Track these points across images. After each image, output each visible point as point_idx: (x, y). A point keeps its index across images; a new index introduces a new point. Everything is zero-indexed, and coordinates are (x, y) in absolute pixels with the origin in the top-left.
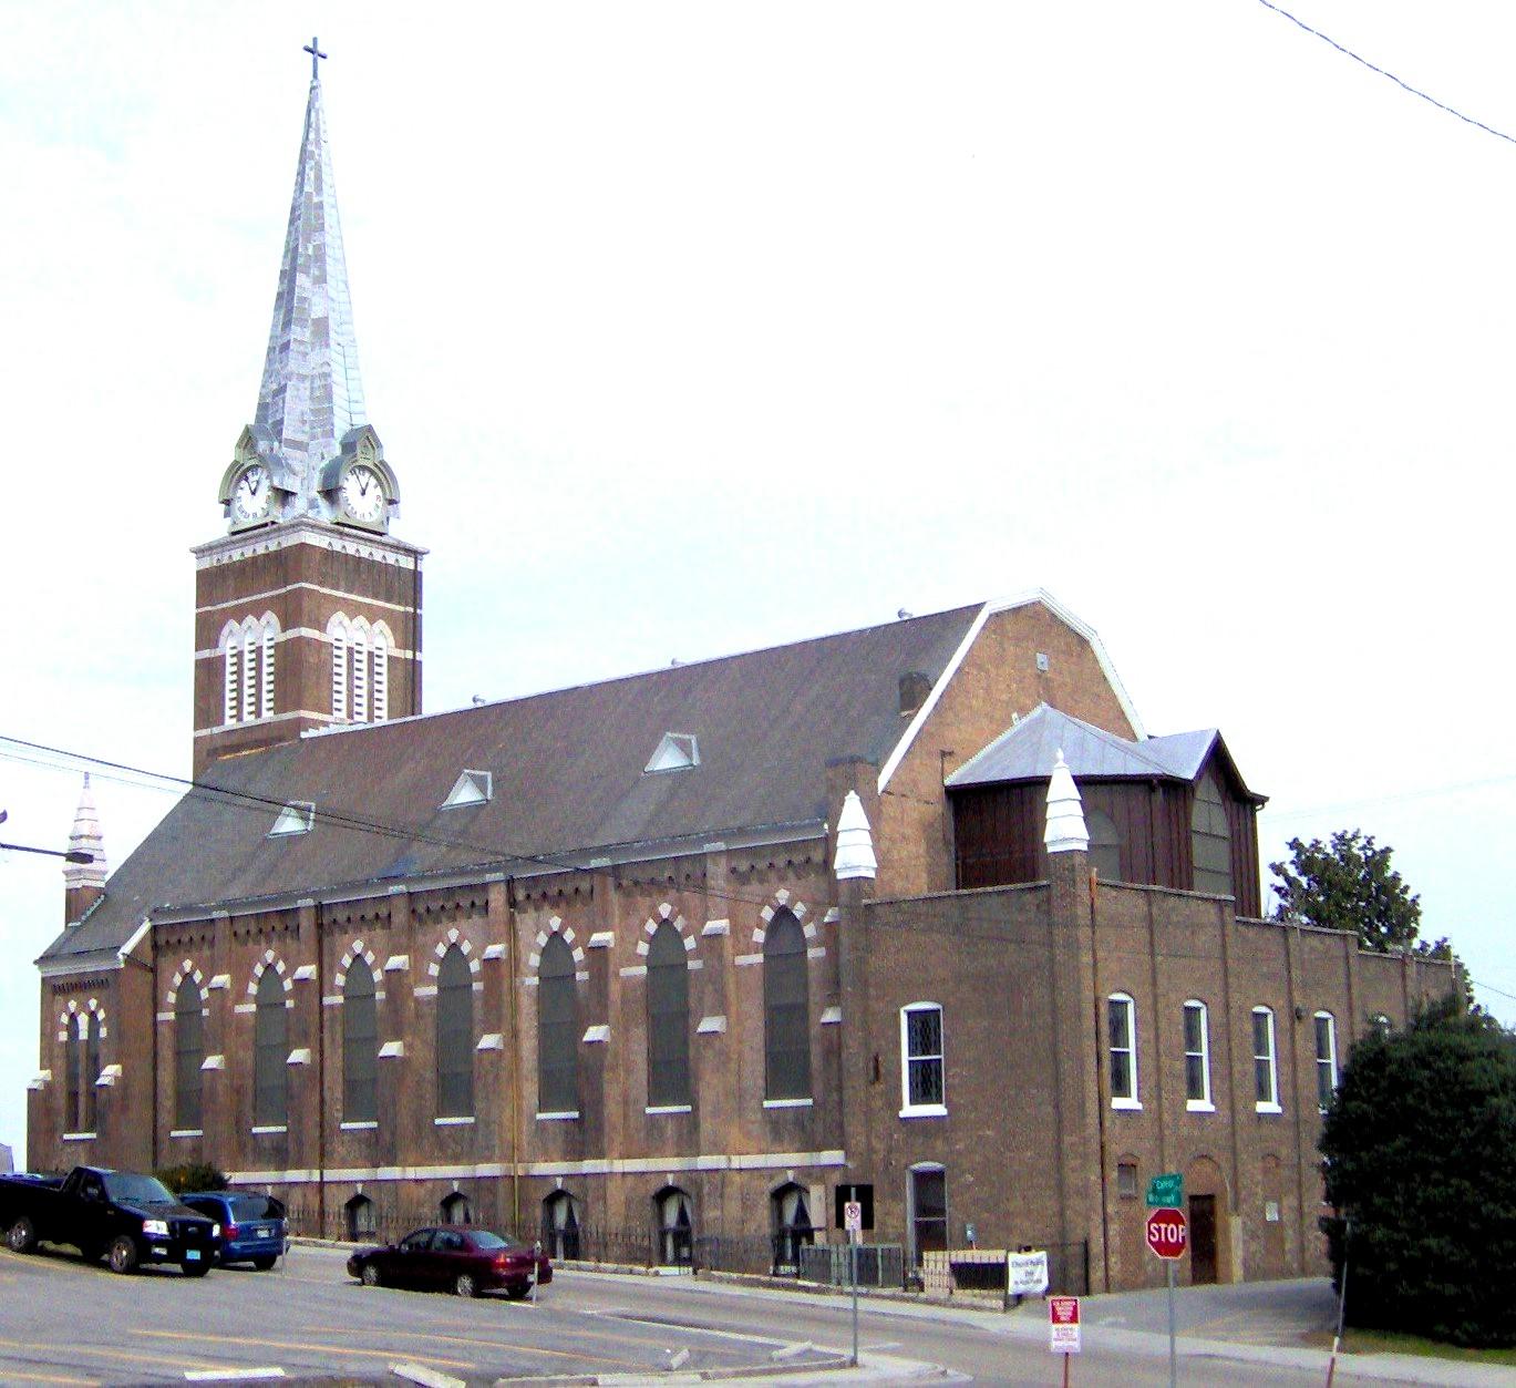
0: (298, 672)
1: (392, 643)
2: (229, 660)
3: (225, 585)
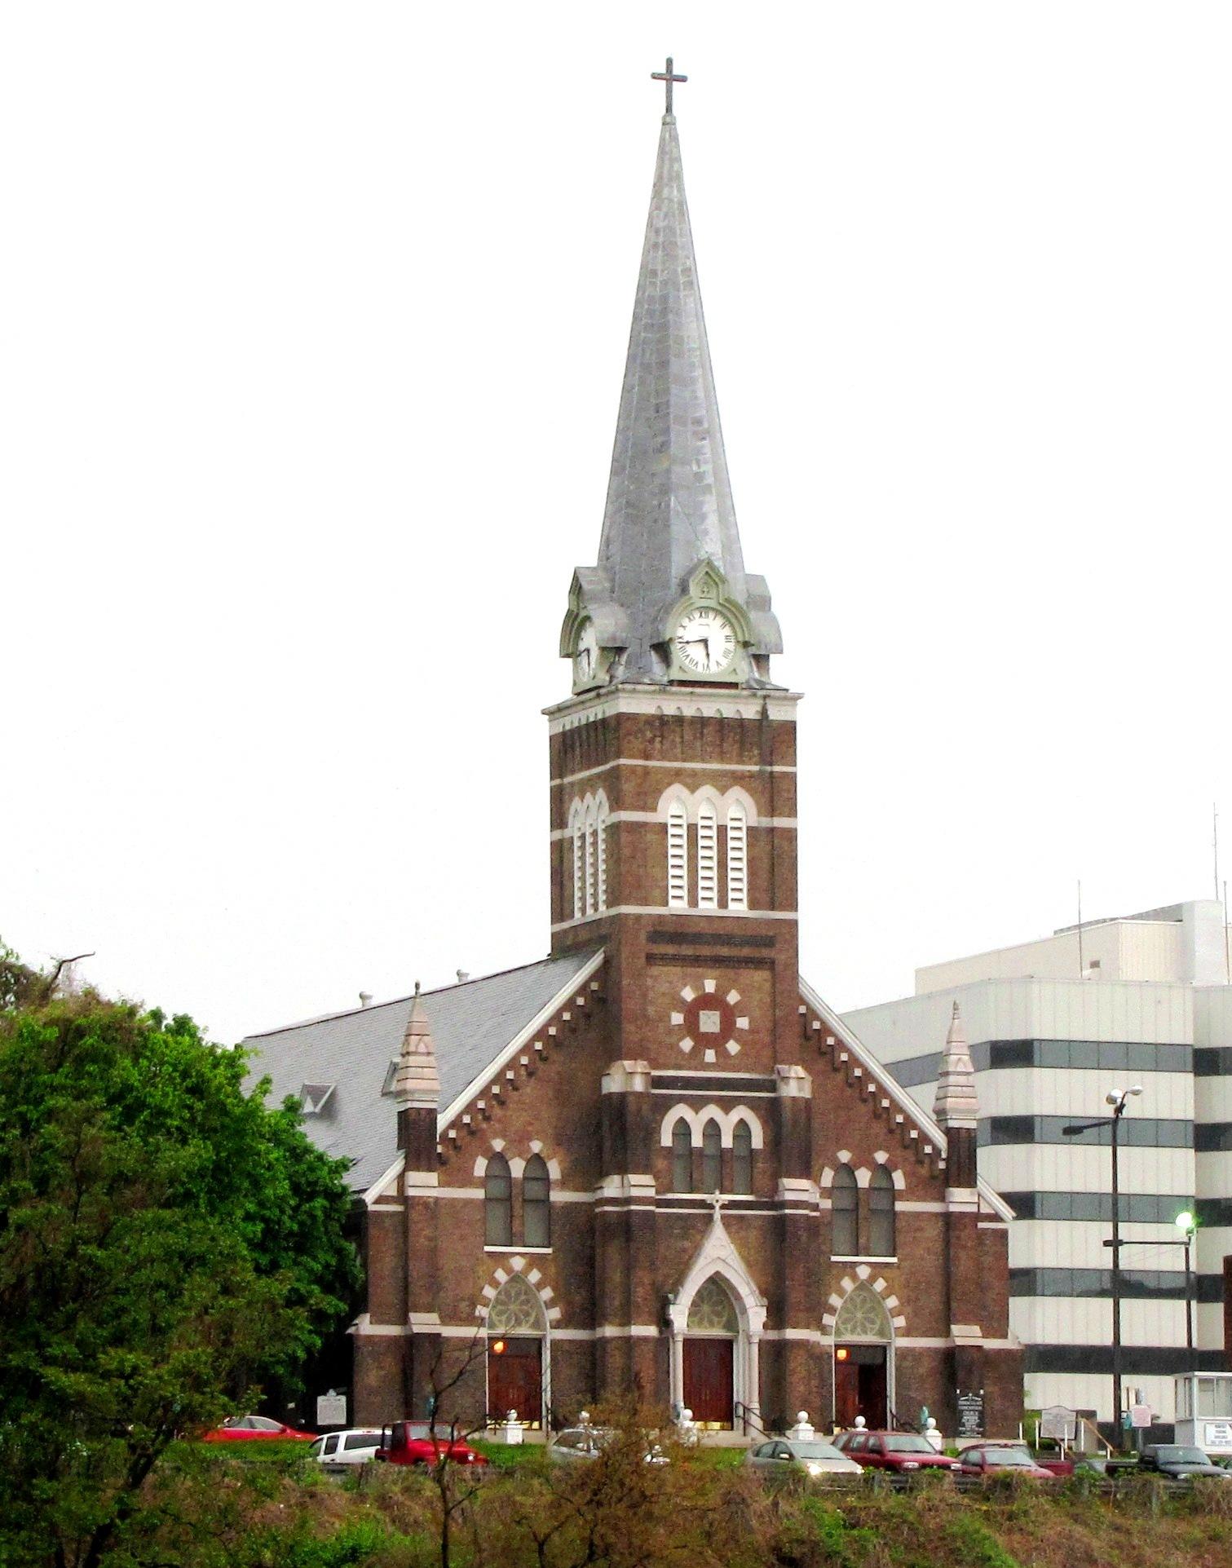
0: (634, 857)
1: (753, 810)
2: (577, 843)
3: (586, 748)
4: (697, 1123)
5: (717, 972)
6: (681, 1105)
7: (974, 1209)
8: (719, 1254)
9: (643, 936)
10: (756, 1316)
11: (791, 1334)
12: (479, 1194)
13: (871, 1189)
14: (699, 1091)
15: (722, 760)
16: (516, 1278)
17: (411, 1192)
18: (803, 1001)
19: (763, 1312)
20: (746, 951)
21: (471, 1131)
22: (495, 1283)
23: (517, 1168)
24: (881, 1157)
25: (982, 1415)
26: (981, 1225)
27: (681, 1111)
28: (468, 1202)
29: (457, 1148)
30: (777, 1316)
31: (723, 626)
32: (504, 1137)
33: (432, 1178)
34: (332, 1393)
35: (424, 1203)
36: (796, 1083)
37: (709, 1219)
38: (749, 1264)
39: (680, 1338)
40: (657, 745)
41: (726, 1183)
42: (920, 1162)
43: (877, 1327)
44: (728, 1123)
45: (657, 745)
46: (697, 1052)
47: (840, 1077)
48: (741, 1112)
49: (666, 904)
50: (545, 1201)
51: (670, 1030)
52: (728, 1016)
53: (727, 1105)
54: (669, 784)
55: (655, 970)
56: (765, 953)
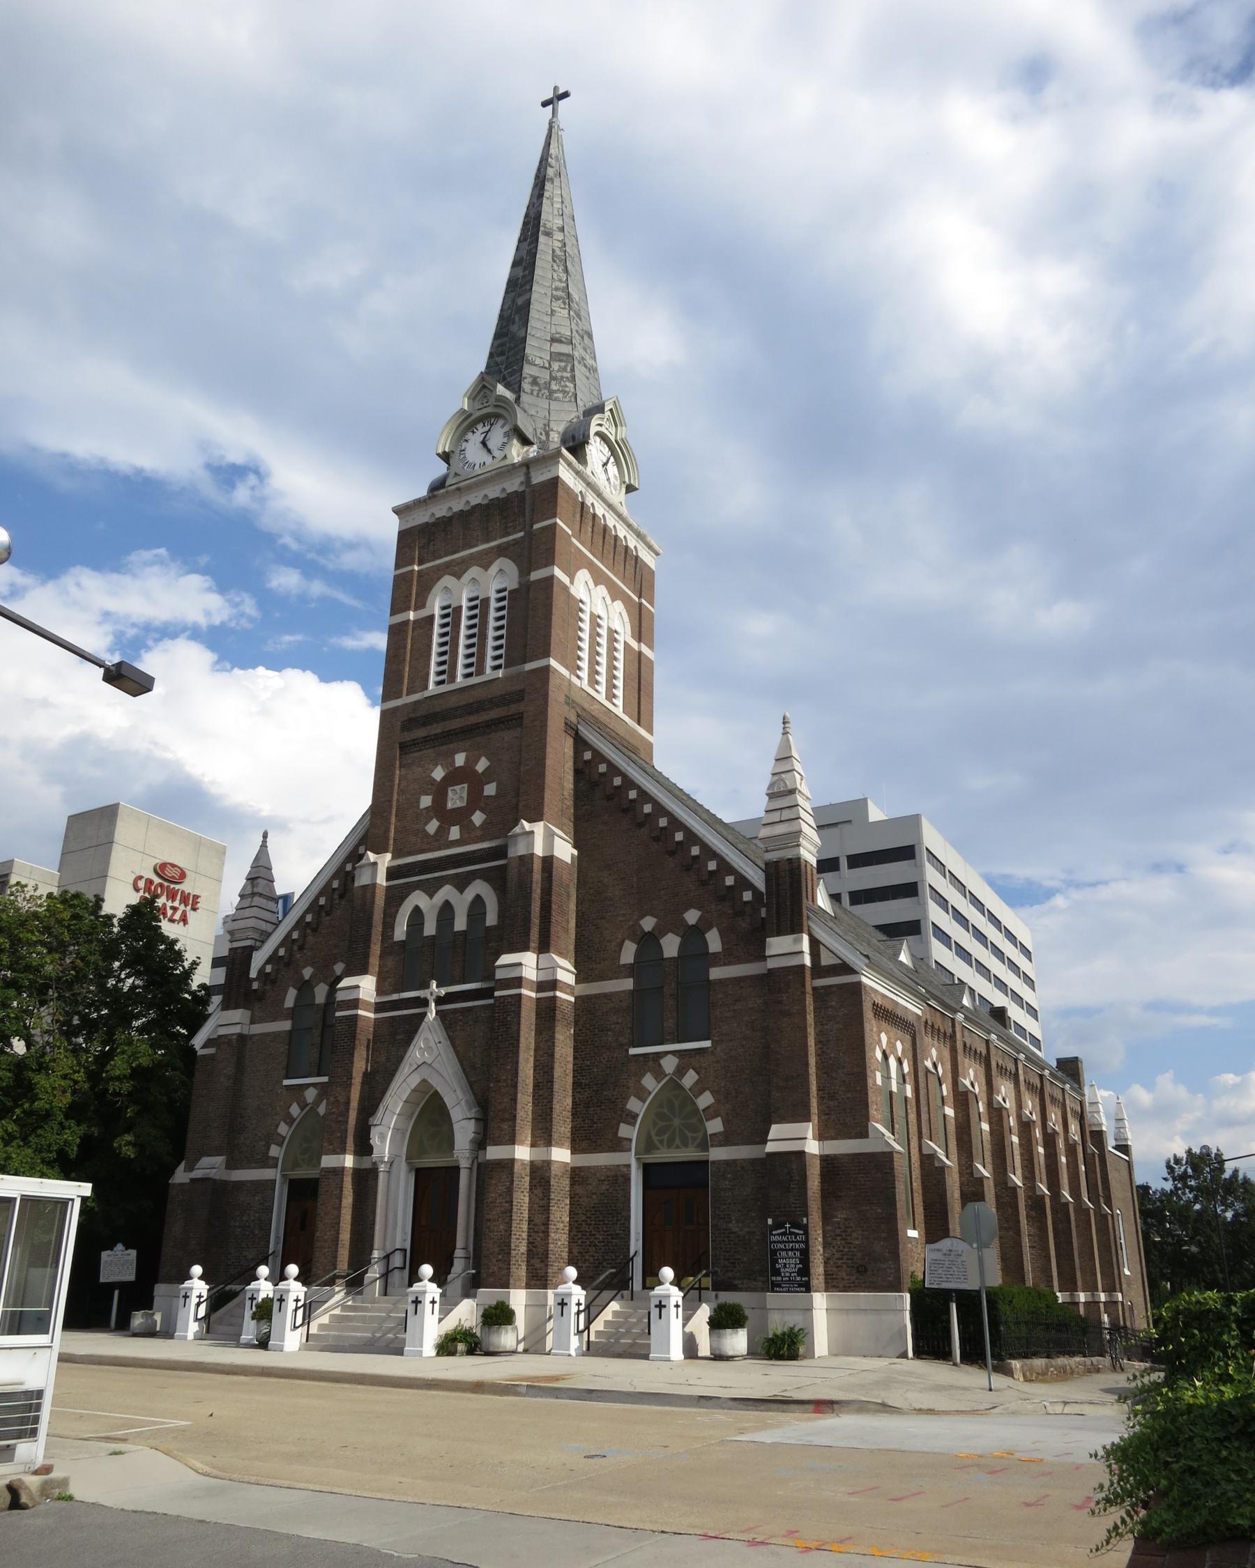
8: (429, 1057)
10: (464, 1132)
15: (488, 541)
20: (494, 714)
22: (290, 1120)
27: (418, 899)
28: (275, 1036)
34: (120, 1247)
46: (443, 831)
48: (479, 888)
53: (461, 884)
54: (439, 579)
56: (513, 709)
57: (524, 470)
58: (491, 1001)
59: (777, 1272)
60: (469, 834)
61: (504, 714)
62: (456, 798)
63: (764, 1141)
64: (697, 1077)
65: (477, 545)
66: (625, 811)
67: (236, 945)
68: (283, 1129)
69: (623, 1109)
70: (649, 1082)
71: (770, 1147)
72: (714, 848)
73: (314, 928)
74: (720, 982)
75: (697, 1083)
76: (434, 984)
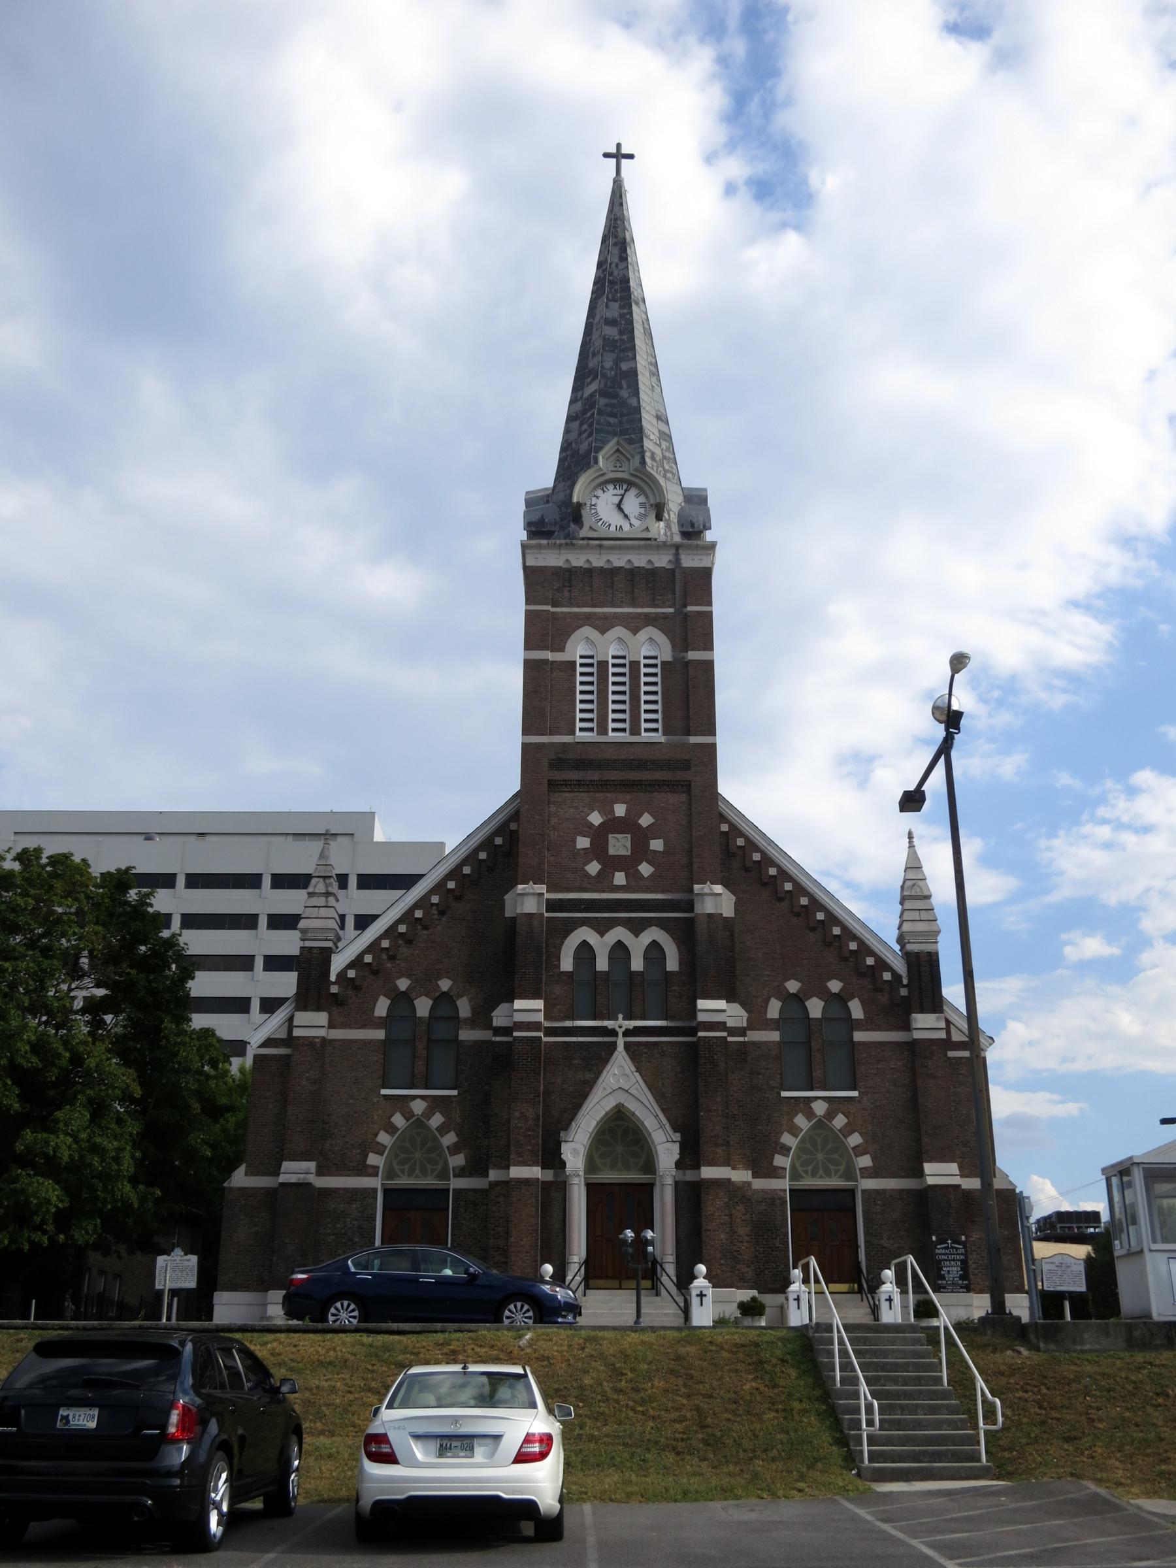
4: (602, 944)
5: (628, 797)
6: (584, 928)
7: (942, 1035)
8: (620, 1084)
9: (545, 763)
10: (667, 1153)
11: (708, 1172)
12: (380, 1034)
13: (825, 1019)
14: (602, 914)
15: (634, 605)
16: (419, 1124)
17: (297, 1033)
18: (723, 818)
19: (676, 1148)
20: (658, 775)
21: (373, 970)
22: (391, 1129)
23: (423, 1007)
24: (835, 986)
25: (965, 1265)
26: (951, 1054)
27: (585, 934)
29: (357, 988)
30: (691, 1156)
31: (637, 496)
32: (409, 977)
33: (322, 1018)
34: (178, 1252)
35: (309, 1042)
36: (717, 900)
37: (613, 1047)
38: (659, 1097)
39: (669, 1181)
40: (566, 594)
41: (818, 1074)
42: (878, 990)
43: (842, 1168)
44: (638, 945)
45: (566, 594)
47: (785, 905)
48: (653, 934)
49: (573, 733)
50: (456, 1041)
51: (576, 854)
52: (641, 838)
53: (637, 928)
54: (578, 627)
55: (558, 797)
56: (679, 776)
57: (673, 551)
58: (694, 1039)
59: (943, 1278)
60: (636, 883)
61: (670, 778)
62: (619, 845)
63: (278, 1174)
64: (846, 1120)
65: (621, 607)
66: (765, 884)
67: (308, 944)
68: (384, 1138)
69: (777, 1142)
70: (801, 1121)
71: (282, 1178)
72: (855, 931)
73: (407, 939)
74: (863, 1043)
75: (846, 1125)
76: (620, 1016)
